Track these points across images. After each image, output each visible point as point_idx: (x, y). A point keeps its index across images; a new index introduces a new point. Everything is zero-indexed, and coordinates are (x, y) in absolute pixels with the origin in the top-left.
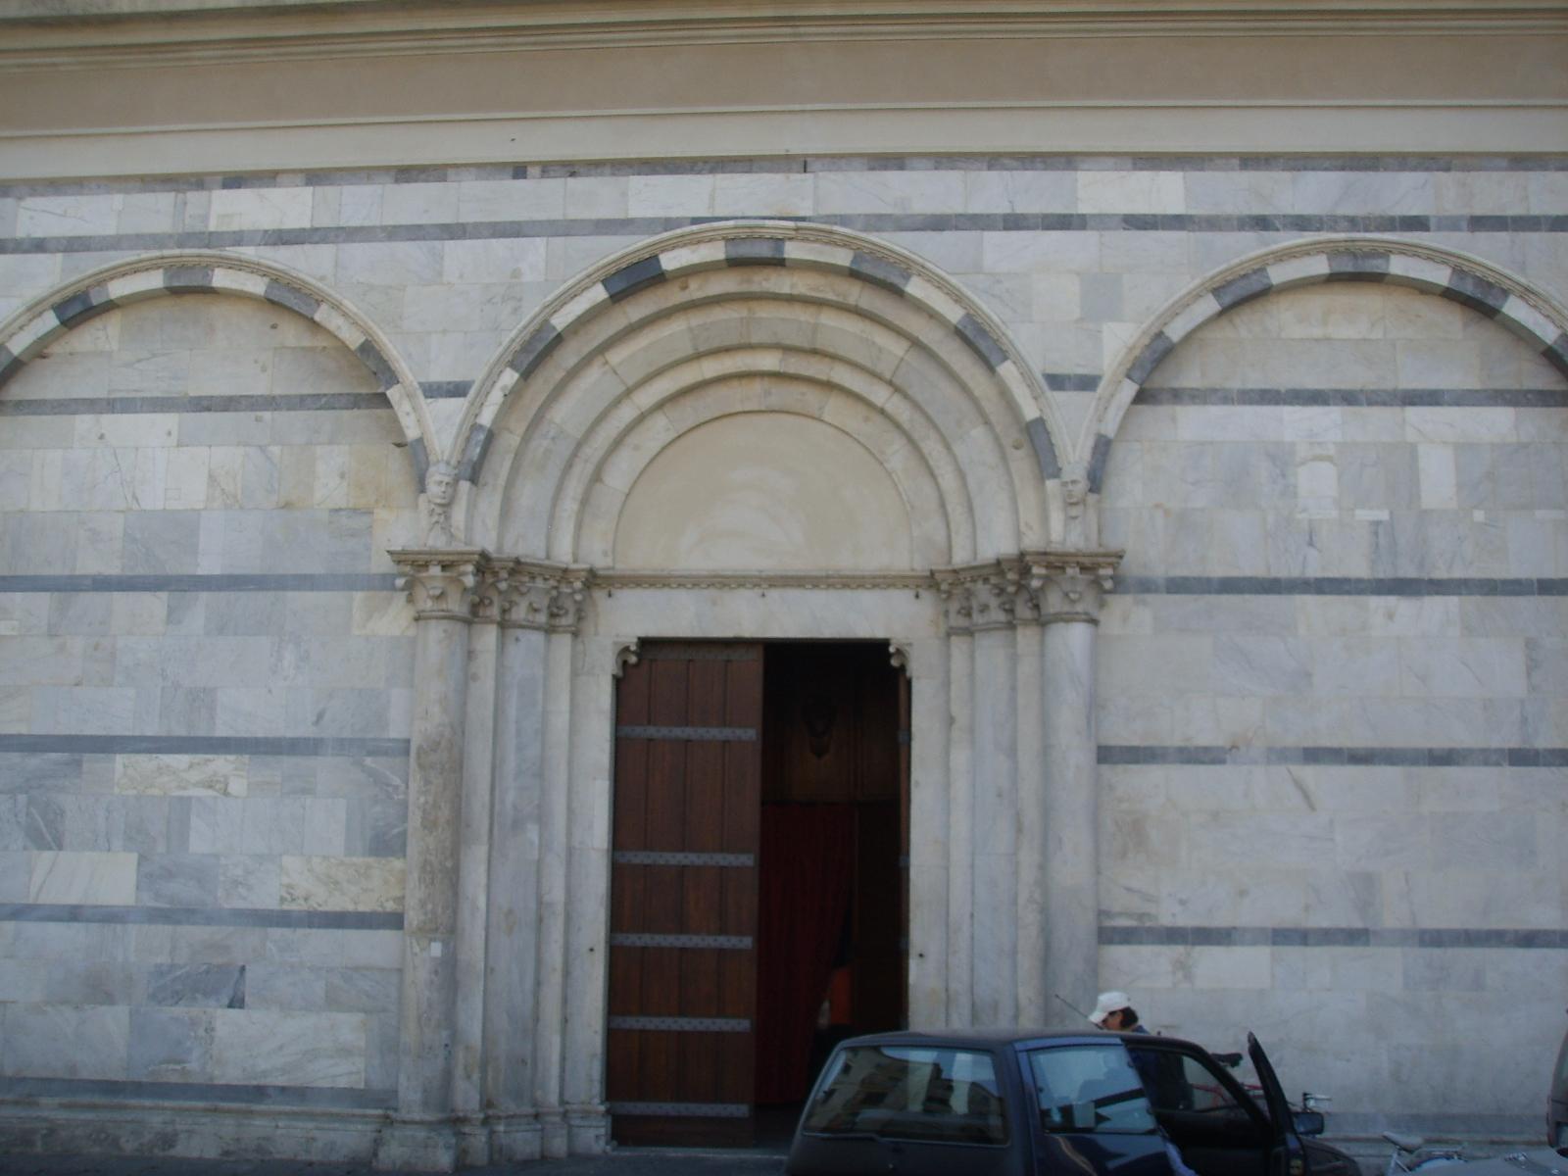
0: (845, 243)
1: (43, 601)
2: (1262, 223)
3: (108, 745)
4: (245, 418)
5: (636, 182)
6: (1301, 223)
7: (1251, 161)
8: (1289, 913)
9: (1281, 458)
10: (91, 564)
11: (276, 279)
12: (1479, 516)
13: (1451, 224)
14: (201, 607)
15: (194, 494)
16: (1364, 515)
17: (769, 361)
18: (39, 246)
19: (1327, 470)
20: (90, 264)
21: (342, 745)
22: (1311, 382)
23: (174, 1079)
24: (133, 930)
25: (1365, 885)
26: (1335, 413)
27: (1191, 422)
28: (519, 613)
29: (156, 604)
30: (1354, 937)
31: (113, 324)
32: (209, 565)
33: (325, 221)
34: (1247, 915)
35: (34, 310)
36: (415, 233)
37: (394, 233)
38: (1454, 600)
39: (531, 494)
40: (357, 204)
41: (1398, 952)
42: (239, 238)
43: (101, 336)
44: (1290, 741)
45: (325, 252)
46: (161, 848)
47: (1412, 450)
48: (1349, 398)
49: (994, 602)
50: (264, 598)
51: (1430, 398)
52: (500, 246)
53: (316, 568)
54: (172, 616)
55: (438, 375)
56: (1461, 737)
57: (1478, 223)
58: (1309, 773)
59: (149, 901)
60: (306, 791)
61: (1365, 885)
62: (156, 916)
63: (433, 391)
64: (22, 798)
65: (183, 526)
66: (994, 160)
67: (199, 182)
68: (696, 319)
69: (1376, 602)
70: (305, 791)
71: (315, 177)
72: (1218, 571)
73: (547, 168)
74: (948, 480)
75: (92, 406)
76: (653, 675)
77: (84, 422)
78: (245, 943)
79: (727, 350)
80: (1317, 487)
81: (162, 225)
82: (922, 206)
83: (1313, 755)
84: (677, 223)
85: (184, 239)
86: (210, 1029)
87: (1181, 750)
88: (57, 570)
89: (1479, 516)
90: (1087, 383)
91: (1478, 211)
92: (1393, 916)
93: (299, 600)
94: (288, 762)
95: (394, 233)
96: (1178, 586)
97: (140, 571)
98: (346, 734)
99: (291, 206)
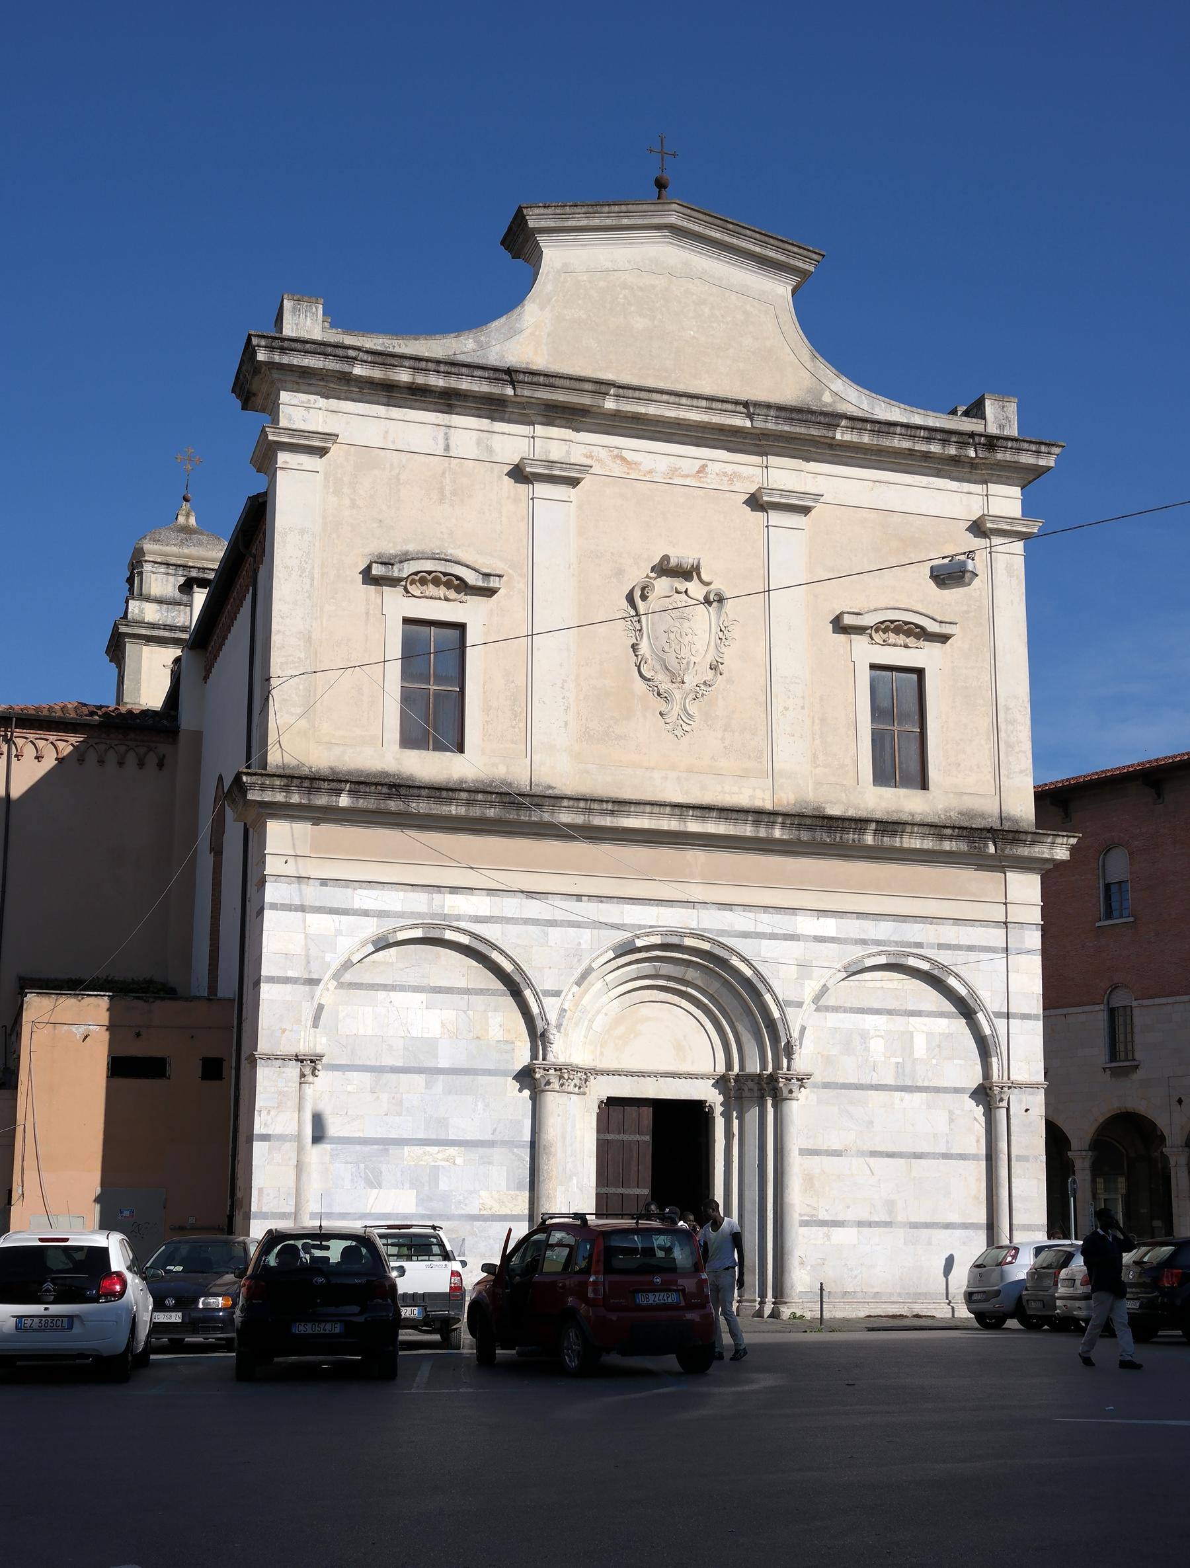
1: (367, 1077)
6: (878, 943)
7: (861, 915)
8: (865, 1216)
9: (864, 1036)
10: (388, 1061)
12: (934, 1061)
13: (931, 946)
14: (441, 1080)
15: (435, 1031)
16: (894, 1060)
18: (365, 913)
19: (881, 1041)
22: (876, 1006)
25: (890, 1205)
26: (884, 1018)
27: (833, 1019)
29: (420, 1079)
30: (888, 1224)
32: (443, 1063)
34: (850, 1216)
36: (536, 922)
37: (527, 921)
40: (511, 906)
42: (458, 918)
44: (865, 1148)
45: (498, 927)
47: (912, 1033)
48: (890, 1012)
50: (467, 1079)
53: (491, 1066)
54: (428, 1086)
57: (941, 946)
58: (872, 1161)
61: (890, 1205)
64: (362, 1166)
65: (431, 1045)
66: (765, 908)
69: (898, 1094)
70: (489, 1163)
72: (841, 1081)
77: (382, 995)
80: (877, 1046)
81: (423, 908)
83: (874, 1154)
84: (644, 927)
85: (434, 916)
89: (934, 1061)
90: (800, 1004)
91: (942, 942)
92: (901, 1217)
95: (527, 921)
96: (827, 1086)
98: (506, 1139)
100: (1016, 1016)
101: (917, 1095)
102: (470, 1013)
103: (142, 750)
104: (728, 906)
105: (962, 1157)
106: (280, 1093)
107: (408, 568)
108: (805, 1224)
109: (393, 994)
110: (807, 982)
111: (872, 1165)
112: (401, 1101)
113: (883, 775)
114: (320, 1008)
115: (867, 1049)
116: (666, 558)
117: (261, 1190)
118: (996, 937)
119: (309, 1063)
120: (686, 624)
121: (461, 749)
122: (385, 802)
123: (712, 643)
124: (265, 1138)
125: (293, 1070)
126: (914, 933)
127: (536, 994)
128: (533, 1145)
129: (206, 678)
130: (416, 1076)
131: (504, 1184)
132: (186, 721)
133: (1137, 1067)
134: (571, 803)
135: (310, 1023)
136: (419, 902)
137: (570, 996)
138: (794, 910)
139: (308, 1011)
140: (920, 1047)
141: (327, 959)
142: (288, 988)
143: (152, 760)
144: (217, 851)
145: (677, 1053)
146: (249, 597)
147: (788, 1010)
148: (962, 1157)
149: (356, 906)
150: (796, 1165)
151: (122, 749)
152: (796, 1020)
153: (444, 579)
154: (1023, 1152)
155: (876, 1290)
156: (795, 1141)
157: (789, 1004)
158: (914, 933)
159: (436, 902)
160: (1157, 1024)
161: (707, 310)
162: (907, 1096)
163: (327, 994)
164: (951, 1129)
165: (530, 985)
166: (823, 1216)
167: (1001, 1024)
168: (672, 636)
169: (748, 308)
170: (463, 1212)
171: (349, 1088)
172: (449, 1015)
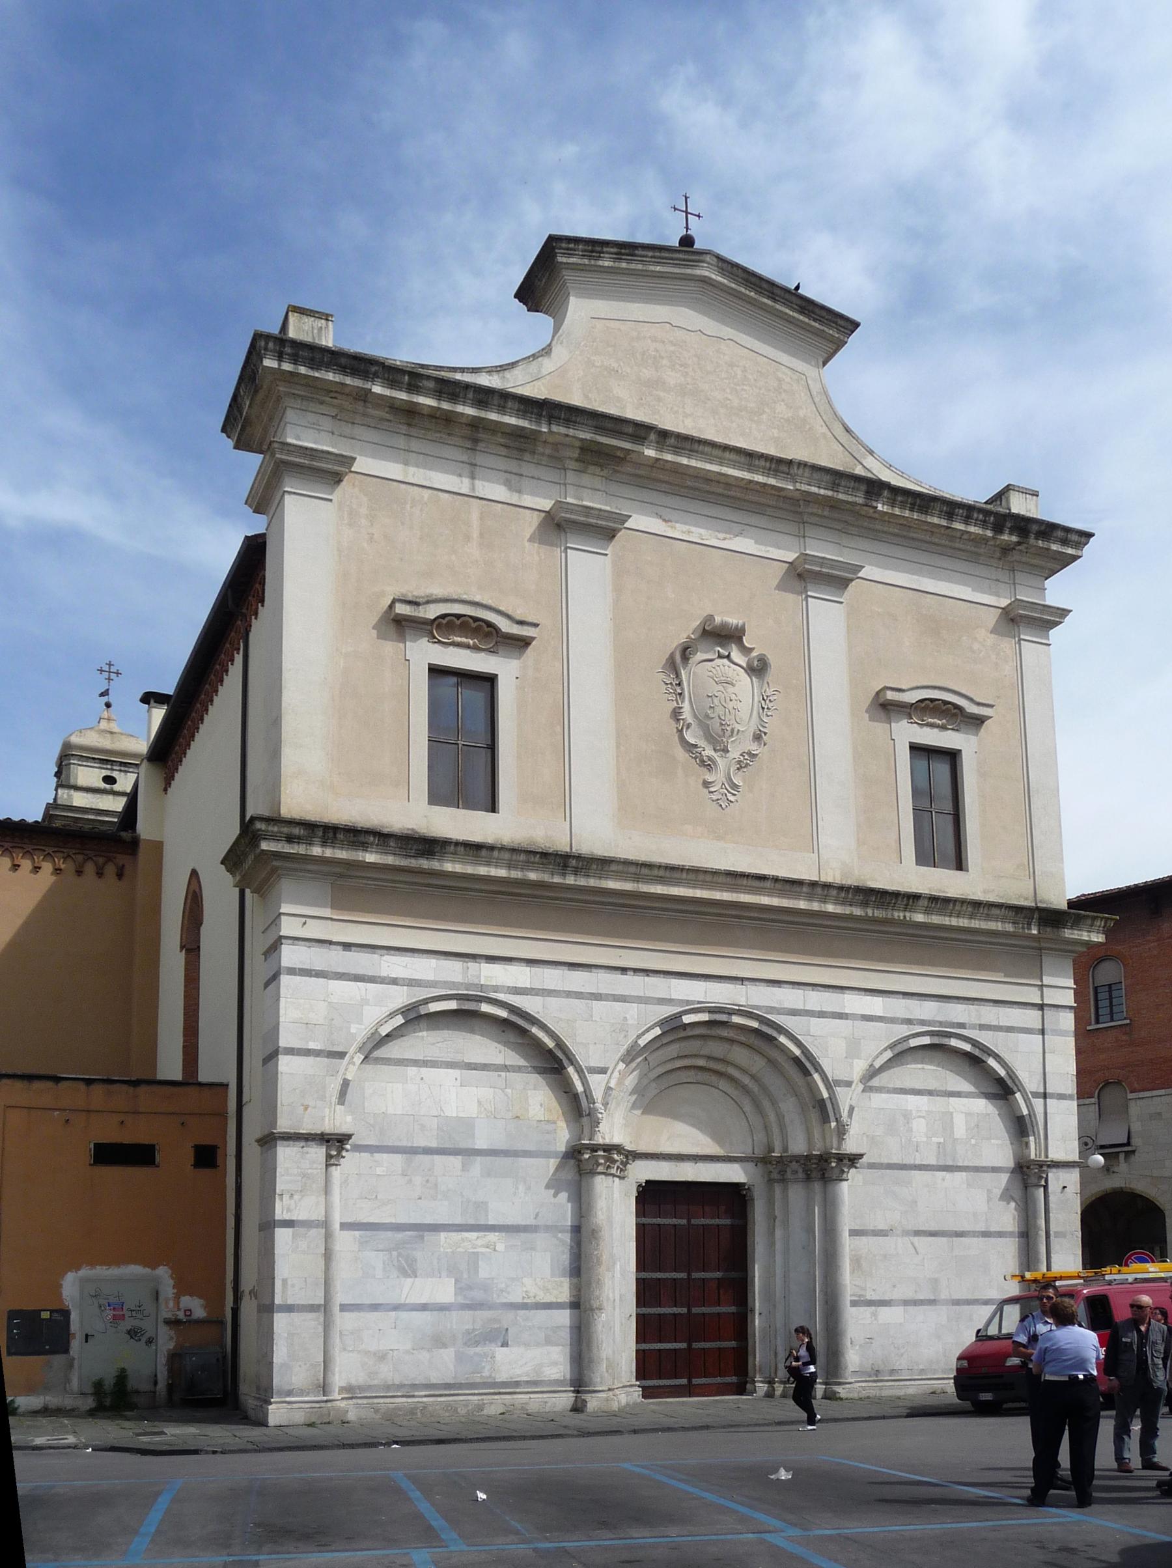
1: (398, 1158)
3: (436, 1228)
4: (493, 1074)
5: (675, 982)
6: (923, 1022)
8: (909, 1295)
9: (907, 1116)
10: (422, 1142)
12: (973, 1141)
13: (973, 1027)
15: (472, 1110)
16: (935, 1140)
17: (701, 1062)
18: (394, 981)
21: (548, 1228)
22: (918, 1086)
23: (478, 1380)
24: (454, 1313)
26: (925, 1098)
27: (878, 1099)
28: (789, 1175)
29: (456, 1161)
30: (932, 1302)
32: (481, 1144)
33: (537, 985)
34: (896, 1295)
35: (392, 1015)
36: (579, 995)
37: (569, 994)
38: (964, 1174)
40: (551, 978)
41: (944, 1308)
42: (496, 989)
44: (910, 1228)
46: (465, 1276)
47: (952, 1114)
48: (930, 1093)
49: (800, 1170)
50: (508, 1161)
54: (465, 1167)
56: (966, 1227)
57: (982, 1027)
58: (916, 1240)
59: (461, 1300)
60: (533, 1249)
64: (395, 1253)
65: (467, 1124)
67: (474, 957)
68: (684, 1044)
72: (885, 1161)
73: (636, 971)
74: (772, 1117)
75: (416, 1063)
77: (412, 1071)
78: (507, 1318)
79: (691, 1056)
80: (919, 1127)
81: (458, 978)
82: (788, 1005)
83: (918, 1233)
84: (693, 1002)
85: (468, 986)
86: (493, 1357)
87: (873, 1231)
88: (405, 1143)
89: (973, 1141)
90: (849, 1084)
93: (523, 1161)
95: (569, 994)
97: (447, 1146)
98: (550, 1223)
100: (1053, 1096)
102: (509, 1091)
103: (101, 860)
105: (1000, 1234)
106: (304, 1175)
107: (432, 612)
108: (854, 1304)
109: (423, 1070)
110: (856, 1061)
111: (917, 1245)
112: (436, 1185)
113: (926, 856)
114: (346, 1084)
115: (910, 1130)
116: (710, 618)
117: (285, 1281)
118: (1031, 1018)
119: (335, 1143)
120: (731, 689)
121: (493, 808)
122: (401, 874)
123: (755, 712)
124: (289, 1224)
125: (318, 1153)
126: (958, 1013)
127: (579, 1071)
128: (577, 1230)
129: (165, 790)
130: (451, 1158)
131: (548, 1272)
132: (144, 828)
133: (1134, 1152)
134: (620, 868)
135: (334, 1099)
136: (453, 972)
137: (616, 1074)
138: (842, 988)
139: (334, 1086)
140: (960, 1129)
141: (353, 1031)
142: (311, 1059)
143: (110, 869)
144: (191, 948)
145: (689, 1146)
146: (239, 658)
147: (838, 1090)
148: (1000, 1234)
149: (384, 974)
150: (848, 1245)
151: (80, 858)
152: (845, 1098)
153: (474, 625)
154: (1059, 1229)
155: (921, 1367)
156: (847, 1220)
157: (838, 1083)
158: (958, 1013)
159: (470, 972)
160: (1151, 1112)
161: (739, 372)
163: (352, 1067)
164: (989, 1208)
165: (572, 1061)
166: (871, 1295)
167: (1038, 1104)
168: (716, 701)
169: (780, 375)
170: (505, 1301)
171: (379, 1171)
172: (485, 1093)
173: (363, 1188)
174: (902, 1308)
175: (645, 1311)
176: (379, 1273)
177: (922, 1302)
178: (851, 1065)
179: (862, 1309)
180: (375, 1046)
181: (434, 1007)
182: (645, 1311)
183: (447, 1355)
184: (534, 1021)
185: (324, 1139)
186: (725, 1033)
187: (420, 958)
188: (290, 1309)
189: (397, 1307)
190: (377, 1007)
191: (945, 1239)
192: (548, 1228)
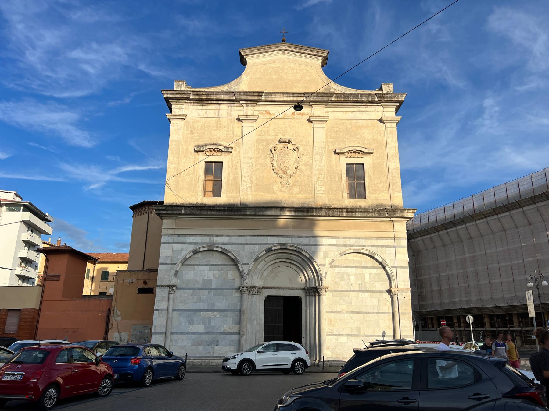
0: (295, 247)
1: (190, 291)
2: (345, 246)
5: (269, 238)
6: (350, 246)
9: (348, 275)
10: (197, 286)
11: (223, 249)
13: (368, 246)
15: (211, 277)
16: (358, 282)
17: (284, 260)
18: (191, 244)
20: (198, 246)
21: (231, 310)
22: (352, 265)
25: (358, 329)
26: (355, 269)
29: (206, 292)
31: (200, 254)
32: (214, 286)
34: (344, 332)
35: (190, 252)
36: (241, 244)
39: (255, 277)
40: (234, 240)
42: (218, 244)
43: (199, 255)
48: (356, 267)
50: (221, 291)
51: (366, 267)
52: (252, 246)
54: (209, 293)
55: (244, 263)
57: (372, 246)
58: (351, 315)
60: (227, 316)
61: (358, 329)
62: (206, 333)
63: (244, 264)
65: (210, 281)
67: (212, 235)
68: (276, 255)
71: (228, 236)
76: (270, 300)
77: (196, 267)
80: (352, 278)
81: (208, 241)
82: (304, 243)
83: (352, 312)
85: (211, 243)
90: (325, 265)
94: (225, 313)
95: (238, 244)
99: (225, 239)
100: (399, 267)
101: (367, 293)
104: (301, 237)
114: (177, 272)
115: (349, 279)
117: (155, 326)
118: (391, 242)
119: (172, 288)
124: (157, 310)
131: (231, 323)
135: (173, 276)
136: (206, 240)
139: (173, 272)
140: (367, 278)
142: (167, 266)
157: (321, 265)
158: (363, 242)
162: (363, 294)
167: (394, 270)
171: (185, 295)
172: (216, 272)
173: (184, 300)
174: (346, 337)
175: (266, 335)
176: (183, 324)
177: (354, 335)
178: (325, 260)
179: (332, 337)
180: (185, 261)
181: (201, 250)
182: (266, 335)
183: (201, 348)
184: (229, 252)
185: (169, 286)
186: (287, 251)
187: (197, 236)
188: (156, 333)
189: (188, 333)
190: (186, 251)
191: (362, 315)
192: (231, 310)
